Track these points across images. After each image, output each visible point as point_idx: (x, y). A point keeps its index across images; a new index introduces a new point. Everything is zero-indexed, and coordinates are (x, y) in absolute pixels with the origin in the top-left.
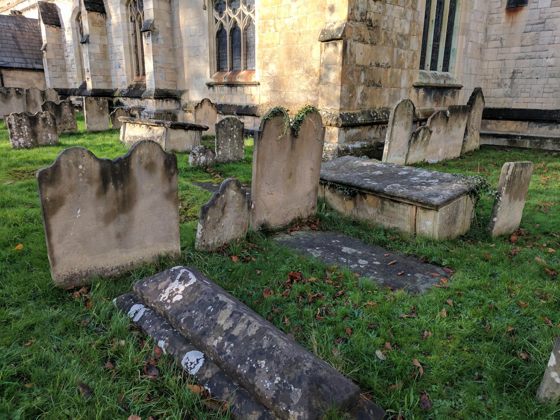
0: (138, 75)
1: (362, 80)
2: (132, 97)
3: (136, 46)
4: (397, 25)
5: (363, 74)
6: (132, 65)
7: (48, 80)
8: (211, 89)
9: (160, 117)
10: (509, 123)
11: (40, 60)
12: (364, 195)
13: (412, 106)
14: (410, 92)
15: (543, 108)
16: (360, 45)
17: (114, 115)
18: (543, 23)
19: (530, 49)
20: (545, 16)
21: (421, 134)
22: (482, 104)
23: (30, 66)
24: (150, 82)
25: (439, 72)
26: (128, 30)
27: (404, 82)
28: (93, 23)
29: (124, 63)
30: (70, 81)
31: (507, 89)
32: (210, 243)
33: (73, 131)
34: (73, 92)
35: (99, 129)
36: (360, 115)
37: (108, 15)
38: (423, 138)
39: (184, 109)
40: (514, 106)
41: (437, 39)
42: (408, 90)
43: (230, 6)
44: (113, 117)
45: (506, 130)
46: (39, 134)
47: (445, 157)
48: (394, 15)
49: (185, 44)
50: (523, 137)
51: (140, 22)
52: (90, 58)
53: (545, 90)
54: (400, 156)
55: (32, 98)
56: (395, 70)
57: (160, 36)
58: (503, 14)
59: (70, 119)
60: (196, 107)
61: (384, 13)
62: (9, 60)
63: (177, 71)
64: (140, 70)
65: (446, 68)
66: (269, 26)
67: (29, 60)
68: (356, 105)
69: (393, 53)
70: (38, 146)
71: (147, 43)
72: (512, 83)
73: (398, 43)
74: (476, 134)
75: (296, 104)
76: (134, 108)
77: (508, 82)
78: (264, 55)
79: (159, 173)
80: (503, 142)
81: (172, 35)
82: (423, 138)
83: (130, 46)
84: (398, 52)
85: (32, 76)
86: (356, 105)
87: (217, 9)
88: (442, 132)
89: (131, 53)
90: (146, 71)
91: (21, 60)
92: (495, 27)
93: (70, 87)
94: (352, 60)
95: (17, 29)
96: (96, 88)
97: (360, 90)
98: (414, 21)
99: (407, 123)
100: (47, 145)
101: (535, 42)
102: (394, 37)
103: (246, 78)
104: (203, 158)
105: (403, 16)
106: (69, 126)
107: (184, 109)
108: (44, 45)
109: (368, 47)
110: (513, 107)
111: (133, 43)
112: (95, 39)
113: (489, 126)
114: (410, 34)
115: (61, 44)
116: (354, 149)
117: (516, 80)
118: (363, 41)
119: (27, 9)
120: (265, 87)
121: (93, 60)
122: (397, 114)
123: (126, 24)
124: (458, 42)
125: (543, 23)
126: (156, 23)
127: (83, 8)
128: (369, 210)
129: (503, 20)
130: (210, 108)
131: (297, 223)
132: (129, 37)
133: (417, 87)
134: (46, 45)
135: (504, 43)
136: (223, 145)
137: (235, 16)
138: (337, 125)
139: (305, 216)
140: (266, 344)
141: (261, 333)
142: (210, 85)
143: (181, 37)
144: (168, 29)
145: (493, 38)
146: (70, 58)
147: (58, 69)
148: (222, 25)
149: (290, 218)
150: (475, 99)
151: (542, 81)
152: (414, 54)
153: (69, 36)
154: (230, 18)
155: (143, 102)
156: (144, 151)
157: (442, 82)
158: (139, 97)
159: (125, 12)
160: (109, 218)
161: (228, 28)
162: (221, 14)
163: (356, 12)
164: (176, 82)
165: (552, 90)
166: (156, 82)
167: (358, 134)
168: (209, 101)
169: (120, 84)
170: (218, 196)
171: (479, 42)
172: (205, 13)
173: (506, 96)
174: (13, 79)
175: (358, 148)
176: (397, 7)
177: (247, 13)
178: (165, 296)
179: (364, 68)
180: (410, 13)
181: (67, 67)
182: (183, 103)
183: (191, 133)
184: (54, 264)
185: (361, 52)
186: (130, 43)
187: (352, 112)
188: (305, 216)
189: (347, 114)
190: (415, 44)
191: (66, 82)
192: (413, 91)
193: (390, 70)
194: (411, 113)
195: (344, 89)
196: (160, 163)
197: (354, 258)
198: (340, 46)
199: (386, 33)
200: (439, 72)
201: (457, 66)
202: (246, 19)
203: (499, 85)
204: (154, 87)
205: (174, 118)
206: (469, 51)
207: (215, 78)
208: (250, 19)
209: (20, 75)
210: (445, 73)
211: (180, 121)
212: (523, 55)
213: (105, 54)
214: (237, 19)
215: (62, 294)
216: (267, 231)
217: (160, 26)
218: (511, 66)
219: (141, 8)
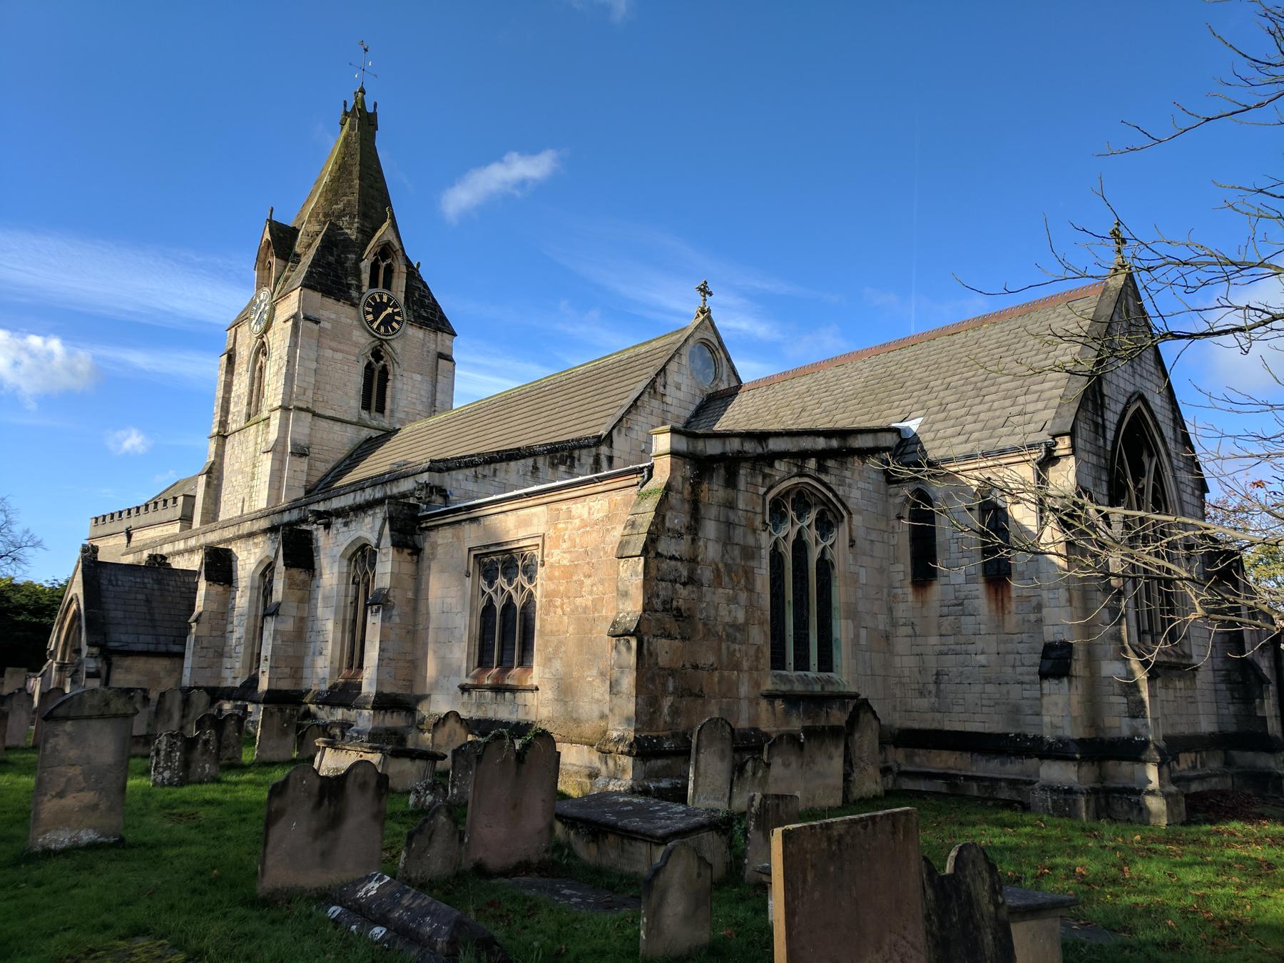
0: (350, 667)
1: (671, 689)
2: (334, 705)
3: (354, 621)
4: (723, 612)
5: (671, 680)
6: (342, 650)
7: (187, 672)
8: (466, 695)
9: (377, 738)
10: (945, 754)
11: (182, 637)
12: (605, 834)
13: (728, 728)
14: (758, 704)
15: (987, 731)
16: (665, 642)
17: (303, 735)
18: (961, 604)
19: (951, 640)
20: (962, 595)
21: (749, 766)
22: (875, 724)
23: (162, 648)
24: (369, 683)
25: (813, 673)
26: (346, 596)
27: (744, 690)
28: (290, 584)
29: (330, 647)
30: (227, 674)
31: (933, 700)
32: (413, 875)
33: (234, 761)
34: (229, 694)
35: (276, 759)
36: (668, 739)
37: (317, 573)
38: (754, 774)
39: (419, 726)
40: (948, 726)
41: (802, 625)
42: (754, 702)
43: (505, 574)
44: (302, 740)
45: (942, 765)
46: (193, 765)
47: (810, 804)
48: (716, 600)
49: (432, 626)
50: (967, 778)
51: (367, 585)
52: (274, 639)
53: (984, 702)
54: (718, 799)
55: (167, 705)
56: (726, 673)
57: (395, 612)
58: (910, 590)
59: (233, 741)
60: (436, 725)
61: (700, 599)
62: (130, 638)
63: (415, 665)
64: (355, 658)
65: (826, 663)
66: (556, 607)
67: (162, 638)
68: (661, 723)
69: (720, 649)
70: (189, 783)
71: (374, 623)
72: (938, 690)
73: (727, 635)
74: (872, 771)
75: (587, 721)
76: (334, 724)
77: (932, 687)
78: (546, 647)
79: (370, 794)
80: (939, 786)
81: (415, 609)
82: (754, 774)
83: (344, 620)
84: (728, 648)
85: (160, 665)
86: (661, 723)
87: (485, 577)
88: (794, 765)
89: (343, 632)
90: (365, 664)
91: (149, 639)
92: (902, 606)
93: (224, 684)
94: (652, 661)
95: (156, 587)
96: (274, 687)
97: (667, 703)
98: (751, 605)
99: (723, 751)
100: (201, 782)
101: (957, 631)
102: (720, 628)
103: (519, 679)
104: (430, 798)
105: (733, 600)
106: (229, 753)
107: (419, 726)
108: (196, 613)
109: (677, 643)
110: (947, 728)
111: (349, 616)
112: (290, 610)
113: (917, 759)
114: (747, 623)
115: (224, 611)
116: (657, 789)
117: (942, 686)
118: (669, 636)
119: (180, 553)
120: (547, 694)
121: (279, 642)
122: (703, 738)
123: (343, 587)
124: (842, 629)
125: (961, 604)
126: (391, 594)
127: (280, 562)
128: (609, 855)
129: (911, 598)
130: (458, 726)
131: (523, 867)
132: (345, 606)
133: (771, 697)
134: (200, 614)
135: (917, 629)
136: (461, 779)
137: (510, 589)
138: (629, 754)
139: (535, 860)
140: (433, 907)
141: (431, 903)
142: (464, 689)
143: (428, 613)
144: (409, 600)
145: (901, 621)
146: (236, 635)
147: (211, 653)
148: (490, 599)
149: (513, 860)
150: (858, 716)
151: (977, 688)
152: (759, 650)
153: (242, 600)
154: (503, 590)
155: (354, 712)
156: (359, 770)
157: (817, 688)
158: (348, 706)
159: (345, 570)
160: (318, 834)
161: (499, 604)
162: (491, 584)
163: (654, 601)
164: (411, 683)
165: (992, 703)
166: (379, 682)
167: (664, 767)
168: (457, 714)
169: (316, 681)
170: (426, 821)
171: (881, 627)
172: (468, 581)
173: (933, 710)
174: (128, 670)
175: (665, 789)
176: (721, 590)
177: (527, 586)
178: (361, 894)
179: (672, 672)
180: (743, 597)
181: (226, 649)
182: (418, 717)
183: (420, 764)
184: (263, 875)
185: (665, 650)
186: (345, 615)
187: (654, 734)
188: (535, 860)
189: (646, 737)
190: (759, 636)
191: (219, 676)
192: (764, 704)
193: (717, 673)
194: (728, 736)
195: (640, 701)
196: (373, 783)
197: (570, 897)
198: (634, 643)
199: (705, 624)
200: (813, 673)
201: (844, 664)
202: (526, 593)
203: (922, 694)
204: (373, 691)
205: (402, 740)
206: (863, 641)
207: (475, 677)
208: (531, 594)
209: (141, 664)
210: (824, 675)
211: (410, 745)
212: (945, 648)
213: (302, 633)
214: (513, 593)
215: (266, 902)
216: (481, 870)
217: (397, 597)
218: (932, 663)
219: (373, 565)
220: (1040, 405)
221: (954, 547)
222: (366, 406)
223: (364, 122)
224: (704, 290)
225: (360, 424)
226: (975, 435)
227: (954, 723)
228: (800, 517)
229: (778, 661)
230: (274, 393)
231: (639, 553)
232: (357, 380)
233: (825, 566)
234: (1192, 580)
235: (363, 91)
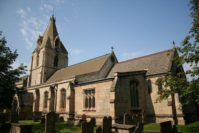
151: (158, 108)
161: (88, 98)
190: (129, 102)
220: (165, 67)
221: (154, 88)
222: (55, 65)
223: (53, 20)
224: (112, 48)
225: (54, 68)
226: (157, 72)
227: (65, 84)
228: (134, 84)
229: (132, 106)
230: (41, 64)
231: (114, 90)
232: (53, 61)
233: (137, 91)
234: (61, 52)
235: (53, 15)
